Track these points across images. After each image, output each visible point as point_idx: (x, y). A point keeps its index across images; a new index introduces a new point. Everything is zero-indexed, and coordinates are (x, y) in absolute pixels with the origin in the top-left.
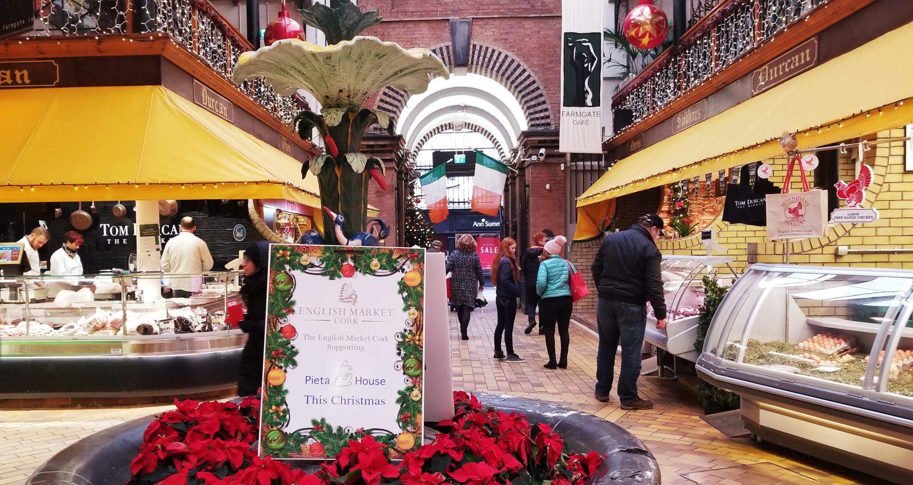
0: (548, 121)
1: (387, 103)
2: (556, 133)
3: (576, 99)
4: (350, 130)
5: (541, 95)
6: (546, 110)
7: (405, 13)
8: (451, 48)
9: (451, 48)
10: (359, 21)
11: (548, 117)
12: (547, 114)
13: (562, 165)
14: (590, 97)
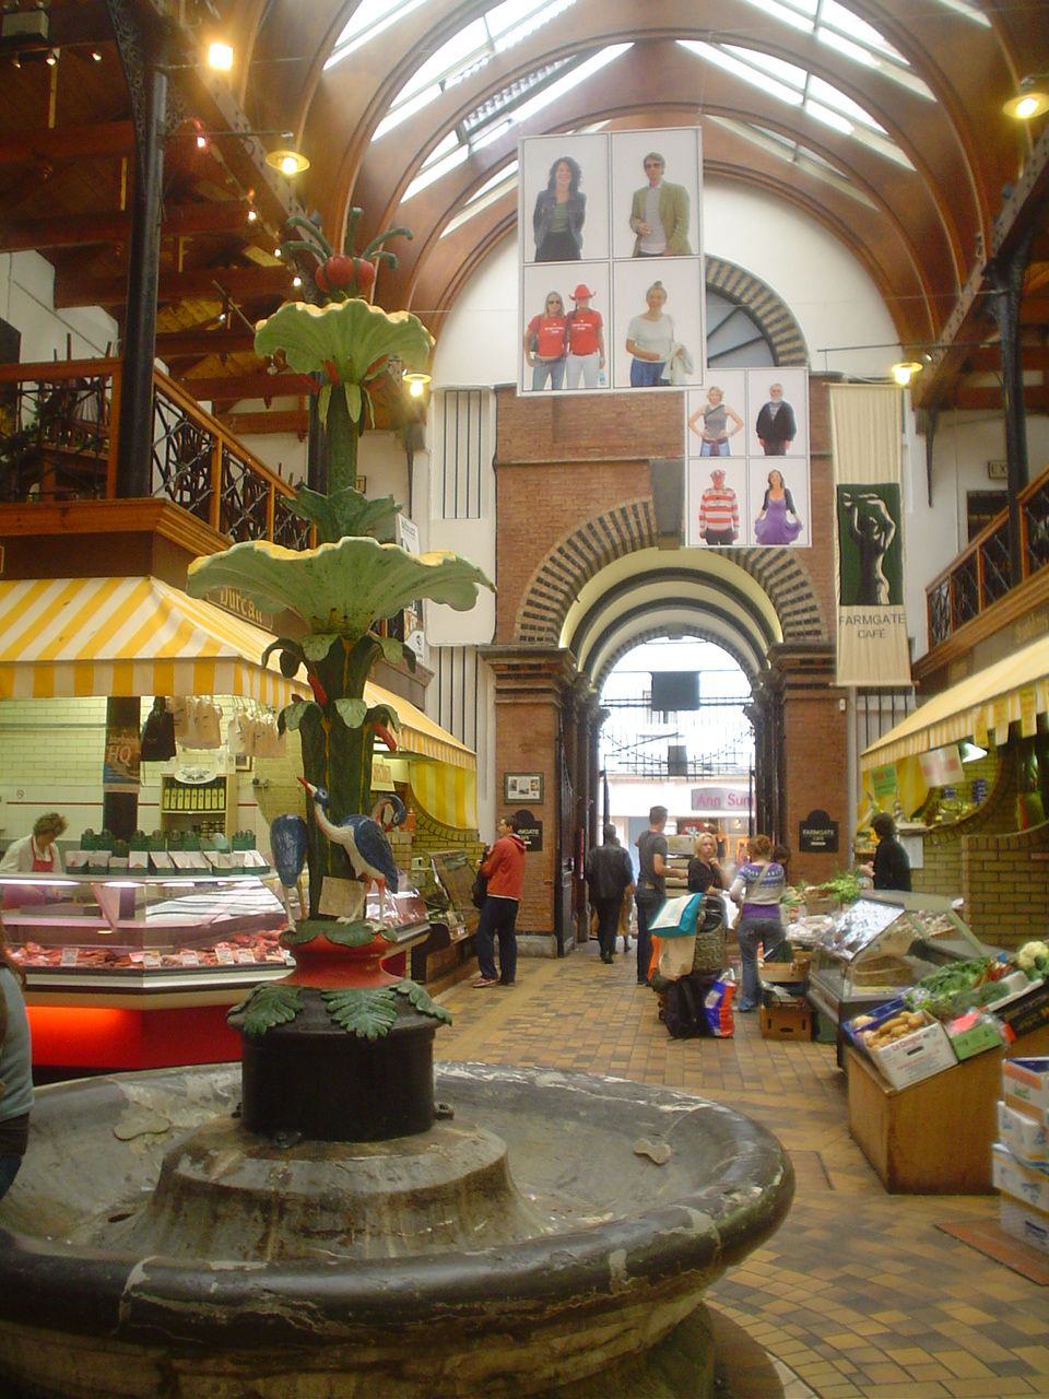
0: (816, 626)
1: (542, 595)
2: (830, 649)
3: (860, 591)
4: (346, 666)
5: (803, 584)
6: (813, 608)
7: (576, 450)
8: (651, 507)
9: (651, 507)
10: (364, 511)
11: (816, 620)
12: (814, 615)
13: (842, 701)
14: (884, 590)
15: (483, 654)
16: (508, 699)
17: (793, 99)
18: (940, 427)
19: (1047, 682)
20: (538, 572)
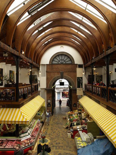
3: (79, 87)
14: (81, 86)
15: (45, 89)
16: (47, 93)
17: (81, 19)
18: (86, 69)
19: (74, 153)
20: (50, 82)
